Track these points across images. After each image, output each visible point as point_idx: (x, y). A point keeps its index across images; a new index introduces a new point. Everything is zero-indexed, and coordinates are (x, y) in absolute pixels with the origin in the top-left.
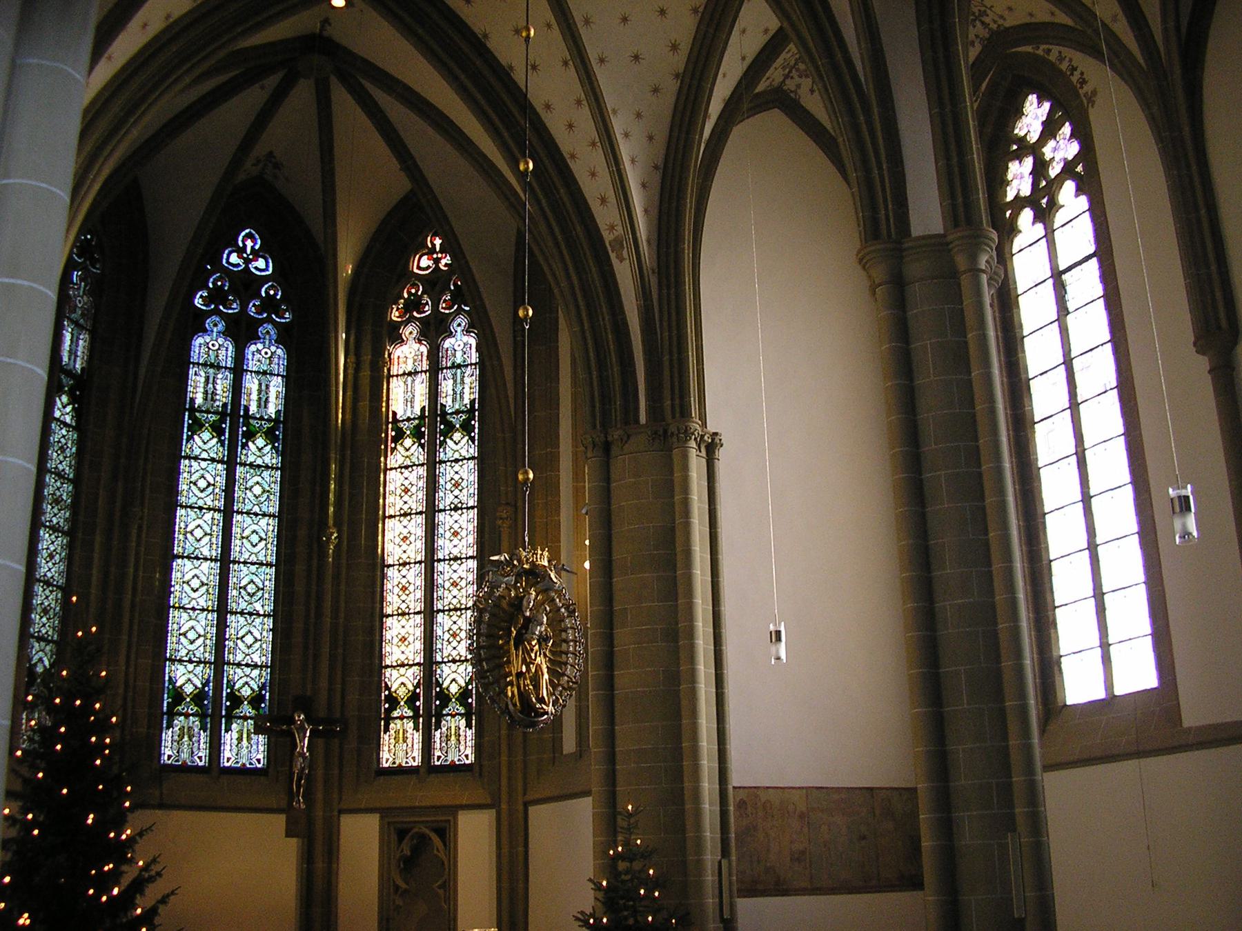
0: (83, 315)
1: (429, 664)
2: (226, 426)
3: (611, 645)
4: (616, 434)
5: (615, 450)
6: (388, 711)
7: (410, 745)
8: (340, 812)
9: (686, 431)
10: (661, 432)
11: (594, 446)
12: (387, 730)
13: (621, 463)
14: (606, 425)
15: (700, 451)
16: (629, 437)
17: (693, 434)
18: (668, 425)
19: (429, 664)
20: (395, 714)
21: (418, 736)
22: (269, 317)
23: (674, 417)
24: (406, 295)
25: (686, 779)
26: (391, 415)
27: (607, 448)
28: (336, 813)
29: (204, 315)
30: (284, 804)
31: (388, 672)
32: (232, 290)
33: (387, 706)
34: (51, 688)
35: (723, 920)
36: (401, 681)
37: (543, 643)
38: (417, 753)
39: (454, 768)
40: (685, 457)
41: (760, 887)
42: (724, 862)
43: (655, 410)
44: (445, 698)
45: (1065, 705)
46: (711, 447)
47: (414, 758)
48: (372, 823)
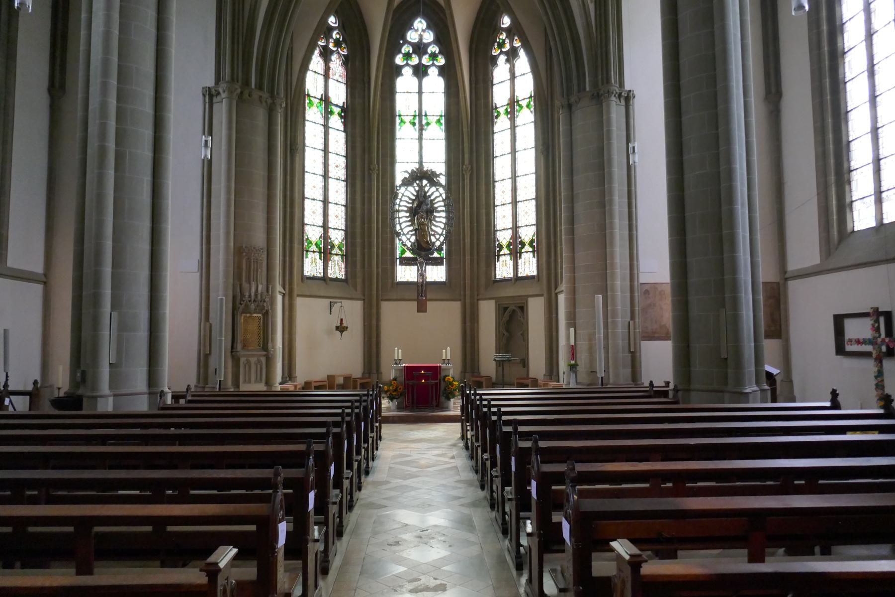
0: (340, 76)
1: (515, 228)
2: (417, 121)
3: (573, 212)
4: (573, 99)
5: (574, 108)
6: (499, 251)
7: (508, 267)
8: (478, 300)
9: (608, 91)
10: (596, 94)
11: (563, 107)
12: (498, 260)
13: (578, 115)
14: (569, 93)
15: (620, 102)
16: (580, 99)
17: (613, 93)
18: (600, 90)
19: (515, 228)
20: (502, 253)
21: (511, 262)
22: (433, 63)
23: (603, 84)
24: (498, 40)
25: (110, 294)
26: (494, 105)
27: (570, 107)
28: (476, 301)
29: (427, 67)
30: (416, 298)
31: (498, 234)
32: (414, 52)
33: (520, 246)
34: (331, 247)
35: (630, 352)
36: (504, 237)
37: (429, 214)
38: (511, 271)
39: (527, 278)
40: (608, 106)
41: (656, 335)
42: (631, 323)
43: (595, 85)
44: (523, 244)
45: (853, 231)
46: (628, 98)
47: (510, 275)
48: (492, 303)
